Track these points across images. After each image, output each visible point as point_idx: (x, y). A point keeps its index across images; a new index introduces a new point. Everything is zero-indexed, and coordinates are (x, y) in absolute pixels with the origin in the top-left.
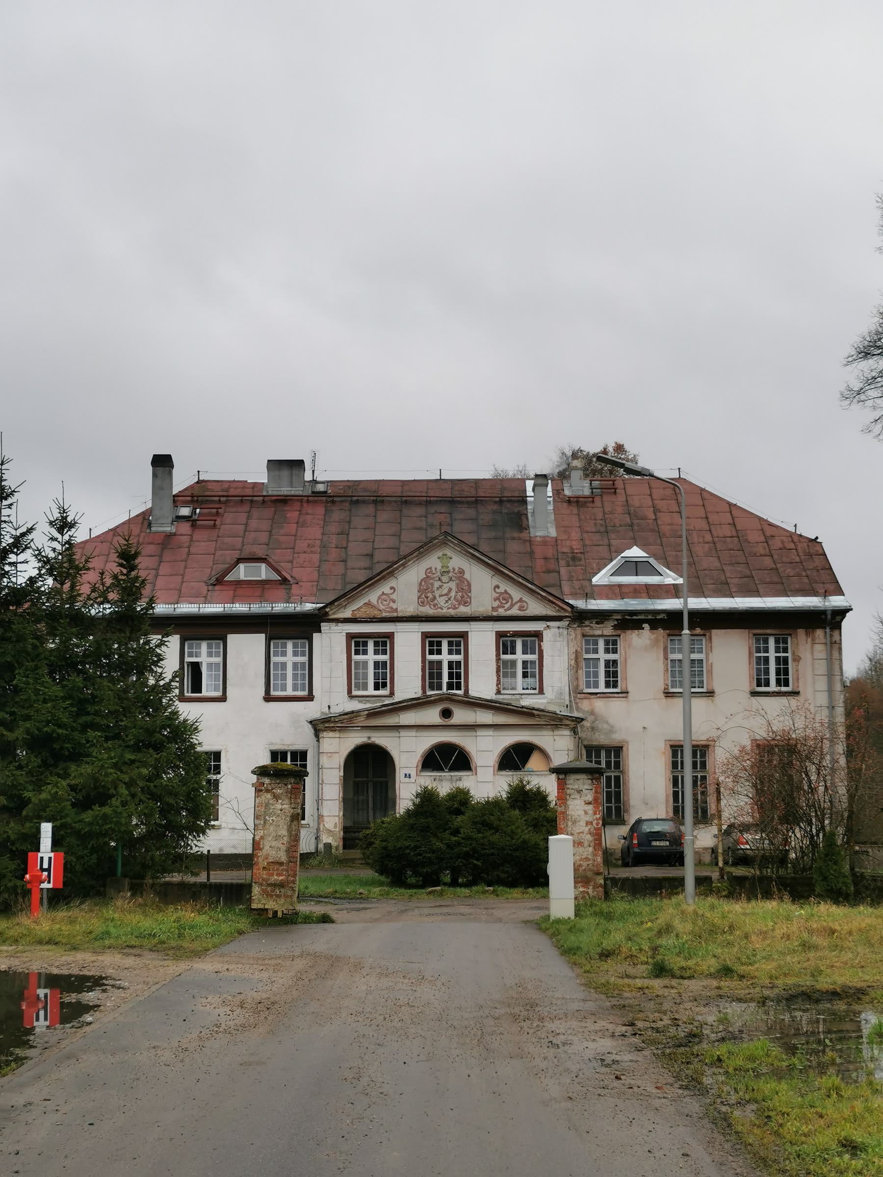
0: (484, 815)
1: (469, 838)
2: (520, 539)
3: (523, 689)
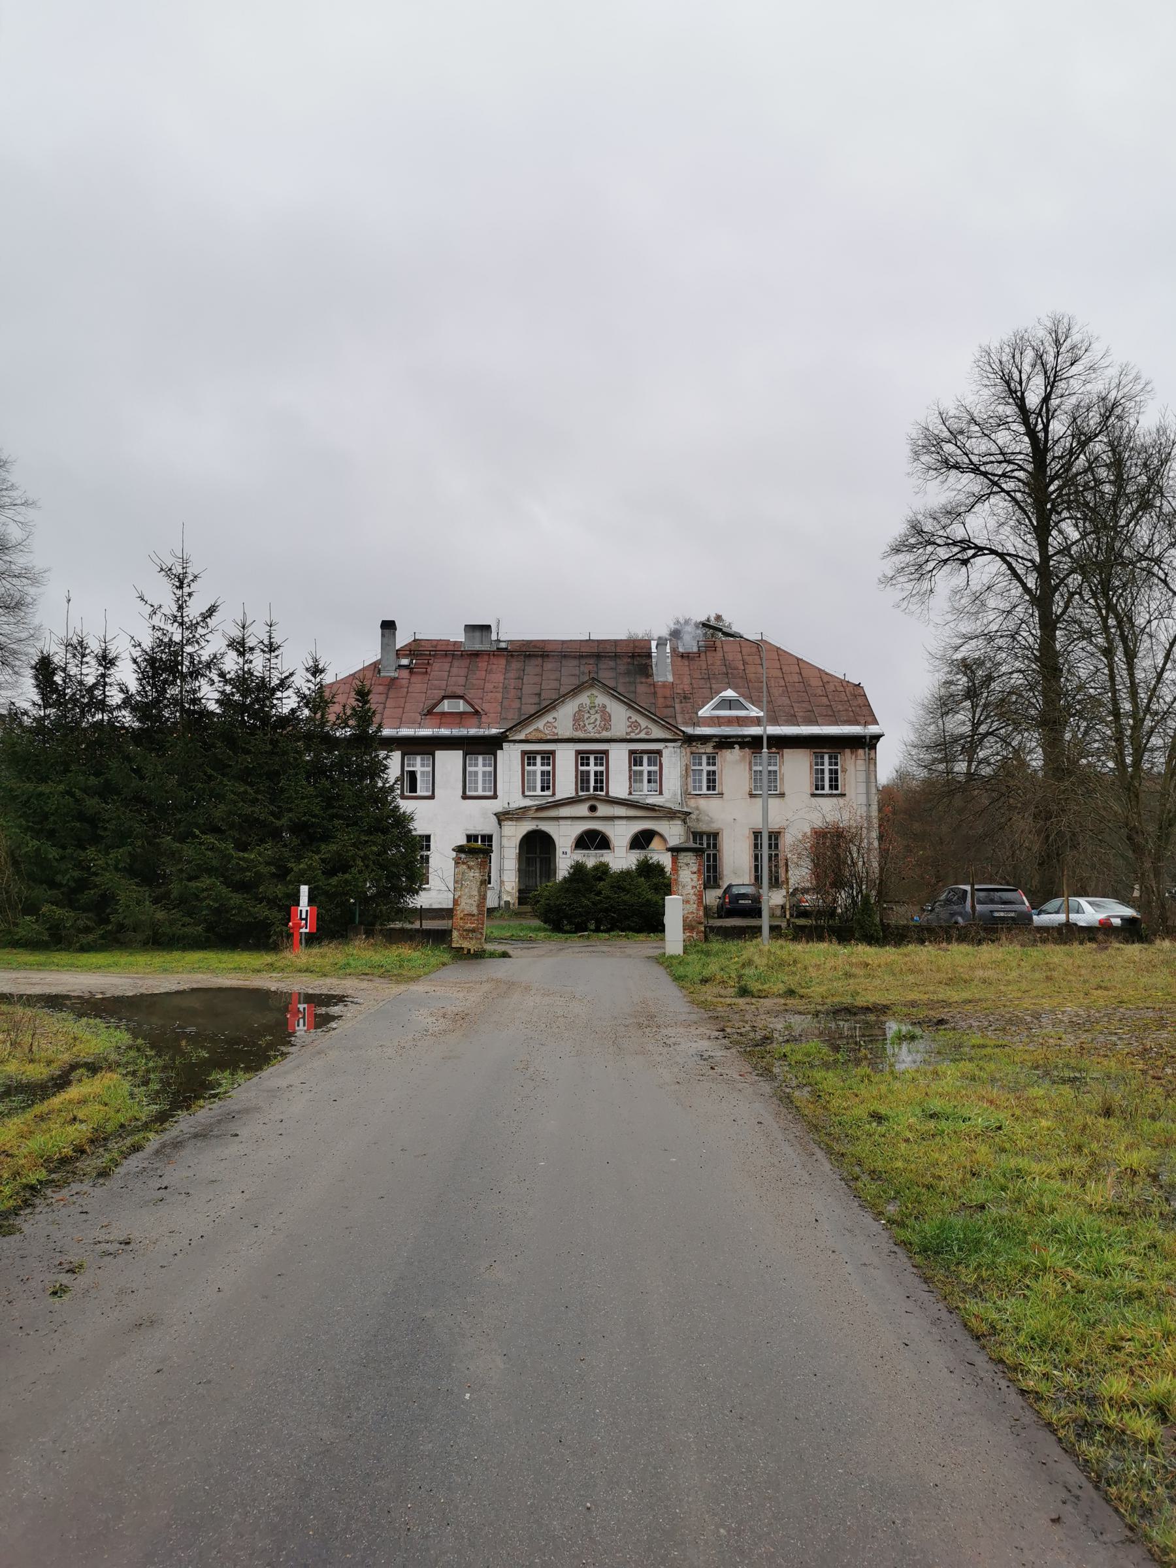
0: (619, 881)
1: (608, 897)
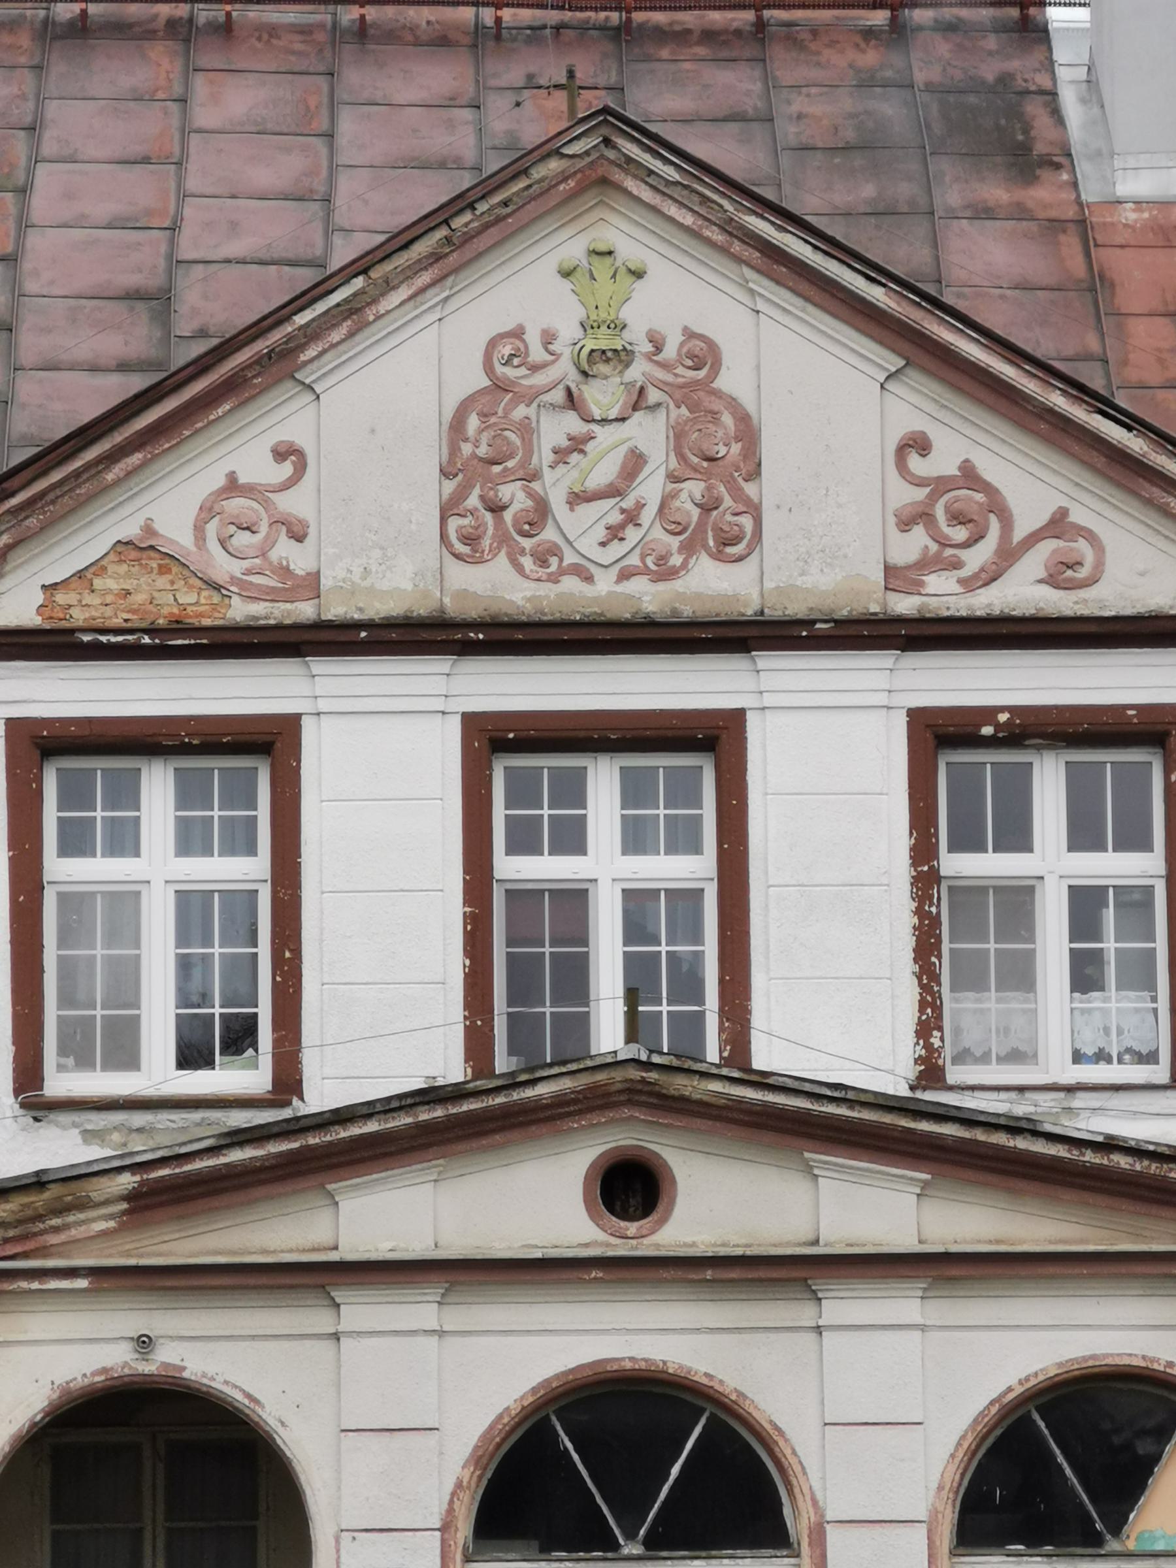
2: (1021, 213)
3: (1078, 1057)
